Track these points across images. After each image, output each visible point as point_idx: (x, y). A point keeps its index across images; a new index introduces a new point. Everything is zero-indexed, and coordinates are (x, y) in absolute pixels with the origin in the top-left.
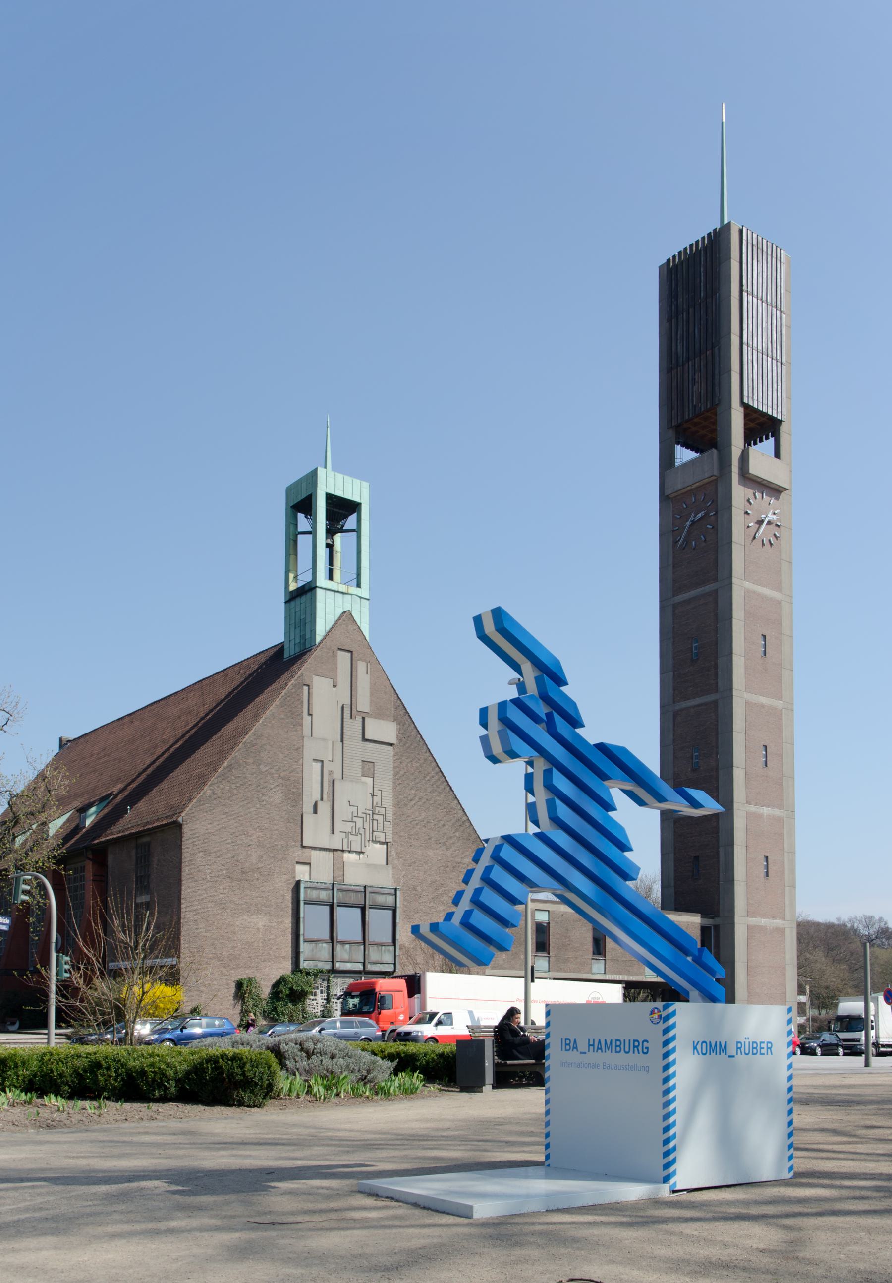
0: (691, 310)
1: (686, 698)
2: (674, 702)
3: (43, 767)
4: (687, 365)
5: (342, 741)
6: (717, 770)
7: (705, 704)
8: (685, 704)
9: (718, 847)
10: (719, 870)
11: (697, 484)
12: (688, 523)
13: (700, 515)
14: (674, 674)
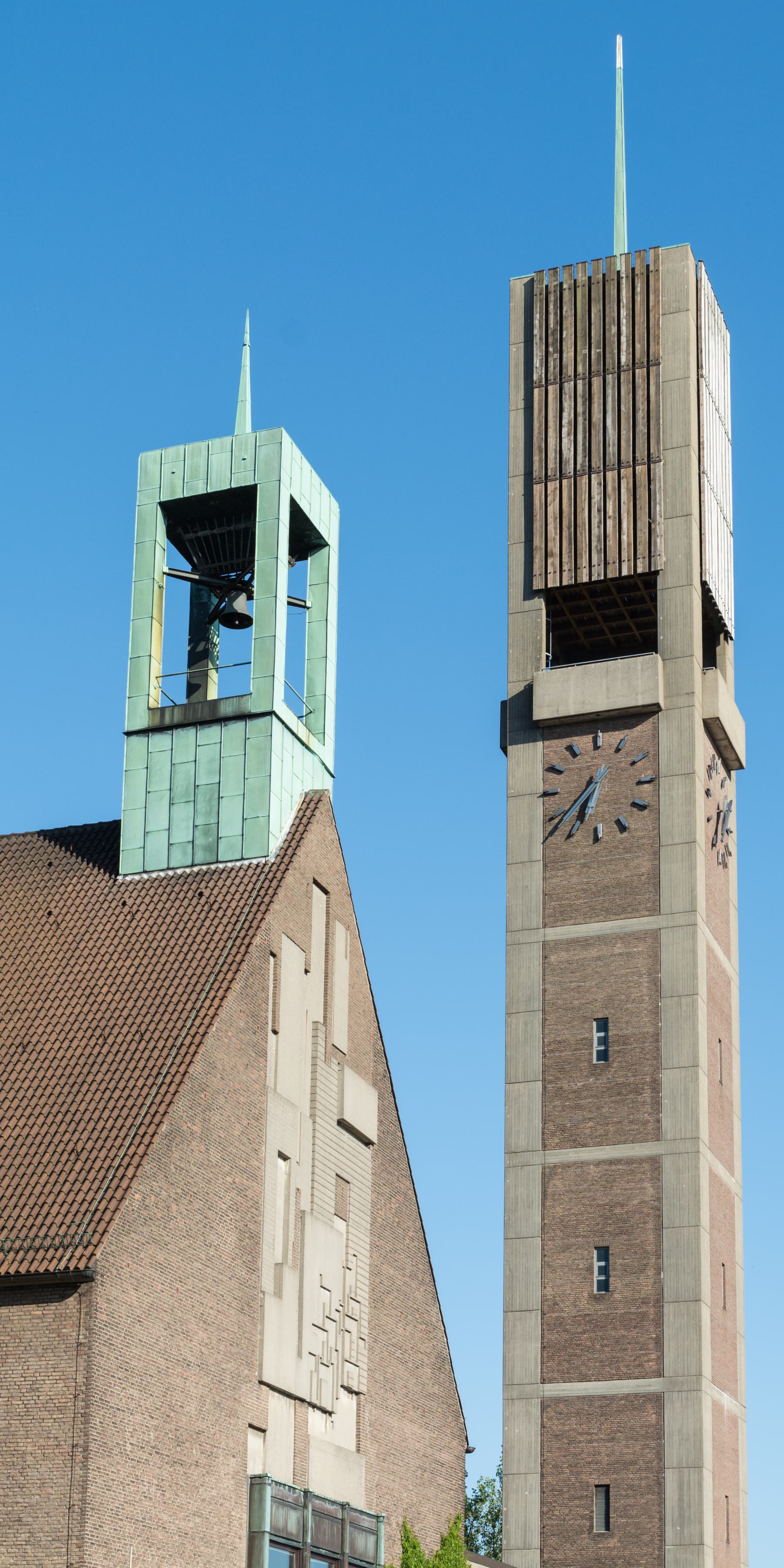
0: (597, 382)
1: (577, 1143)
2: (544, 1146)
4: (585, 479)
5: (313, 1116)
6: (659, 1302)
7: (629, 1161)
9: (661, 1470)
10: (662, 1519)
14: (544, 1088)
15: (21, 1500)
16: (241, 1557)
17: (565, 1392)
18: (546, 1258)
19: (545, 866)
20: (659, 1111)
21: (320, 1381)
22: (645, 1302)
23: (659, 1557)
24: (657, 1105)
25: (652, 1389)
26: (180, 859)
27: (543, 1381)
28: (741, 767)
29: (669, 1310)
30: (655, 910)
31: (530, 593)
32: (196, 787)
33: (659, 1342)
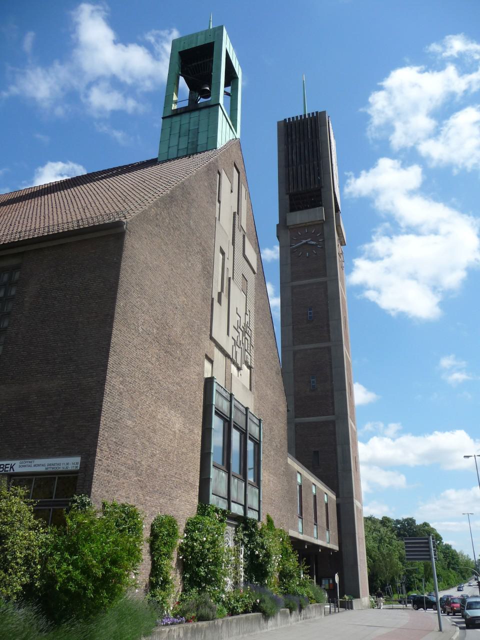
2: (294, 345)
3: (185, 526)
8: (302, 347)
11: (310, 223)
12: (304, 241)
13: (313, 243)
14: (293, 328)
15: (73, 348)
16: (200, 406)
19: (291, 265)
20: (329, 333)
21: (236, 352)
23: (168, 624)
24: (329, 331)
27: (296, 417)
28: (345, 245)
30: (325, 275)
31: (287, 194)
32: (189, 130)
33: (333, 403)
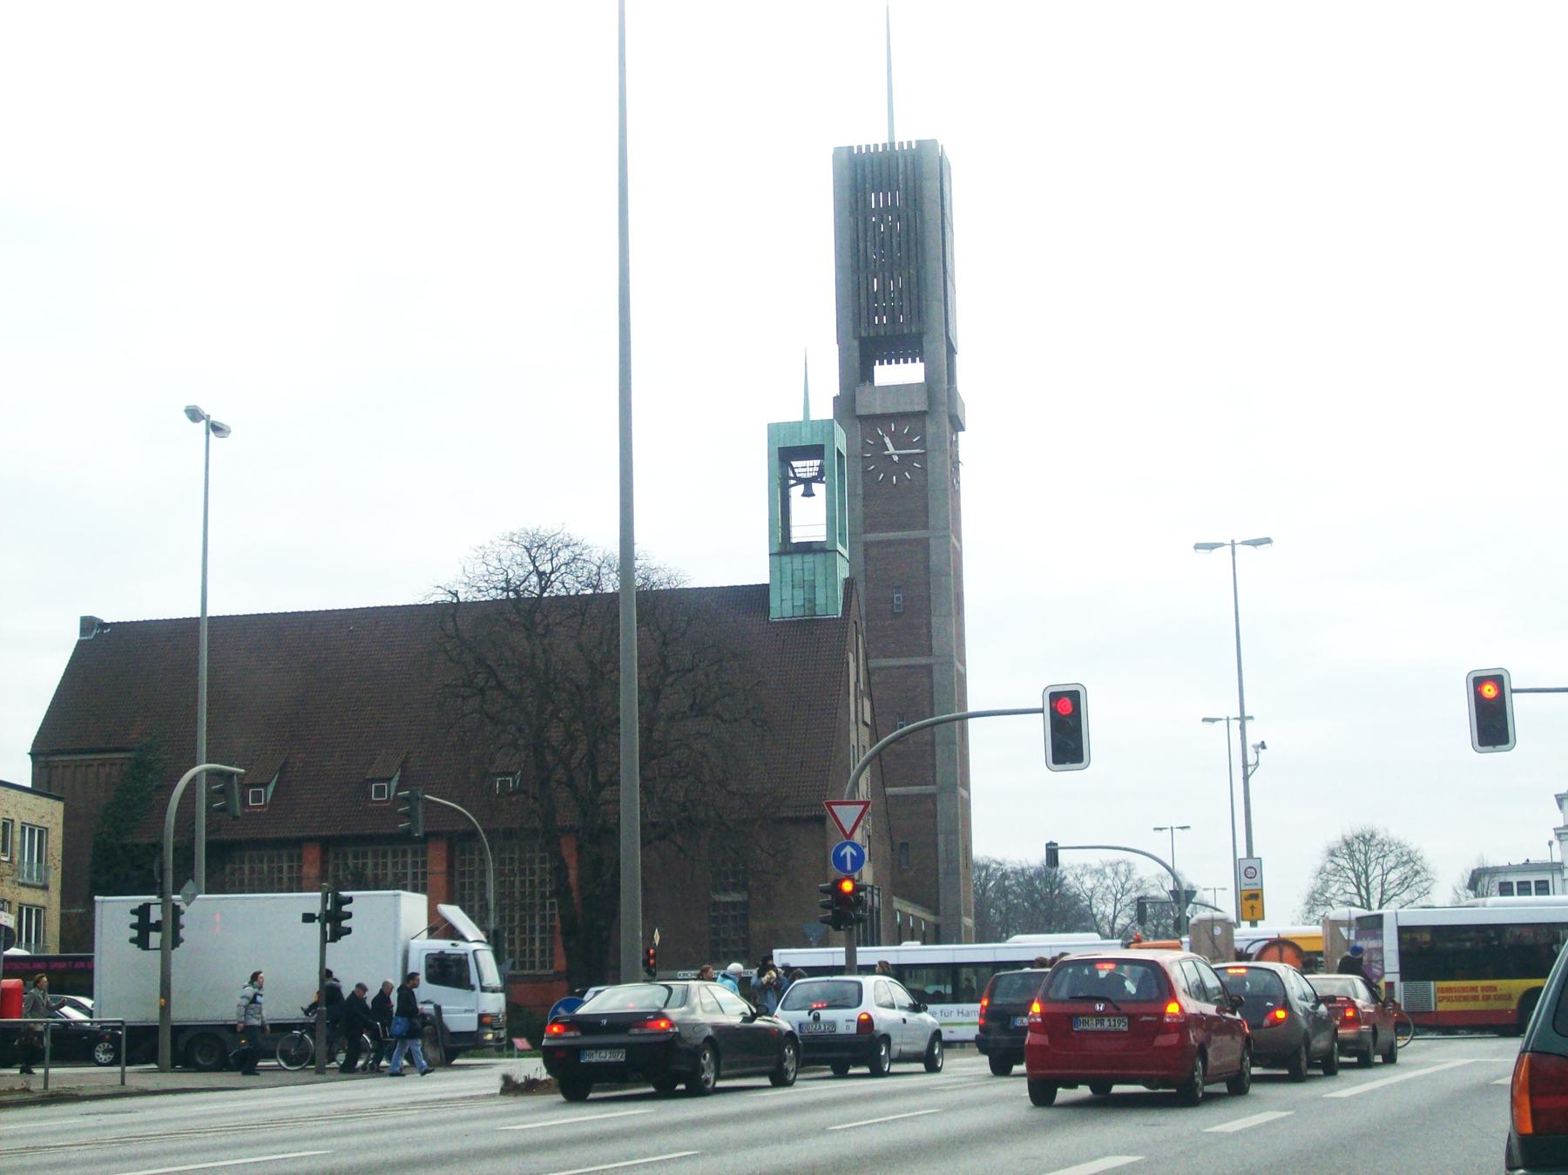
17: (497, 1102)
18: (461, 699)
22: (926, 744)
25: (931, 791)
26: (798, 612)
29: (938, 750)
30: (926, 527)
